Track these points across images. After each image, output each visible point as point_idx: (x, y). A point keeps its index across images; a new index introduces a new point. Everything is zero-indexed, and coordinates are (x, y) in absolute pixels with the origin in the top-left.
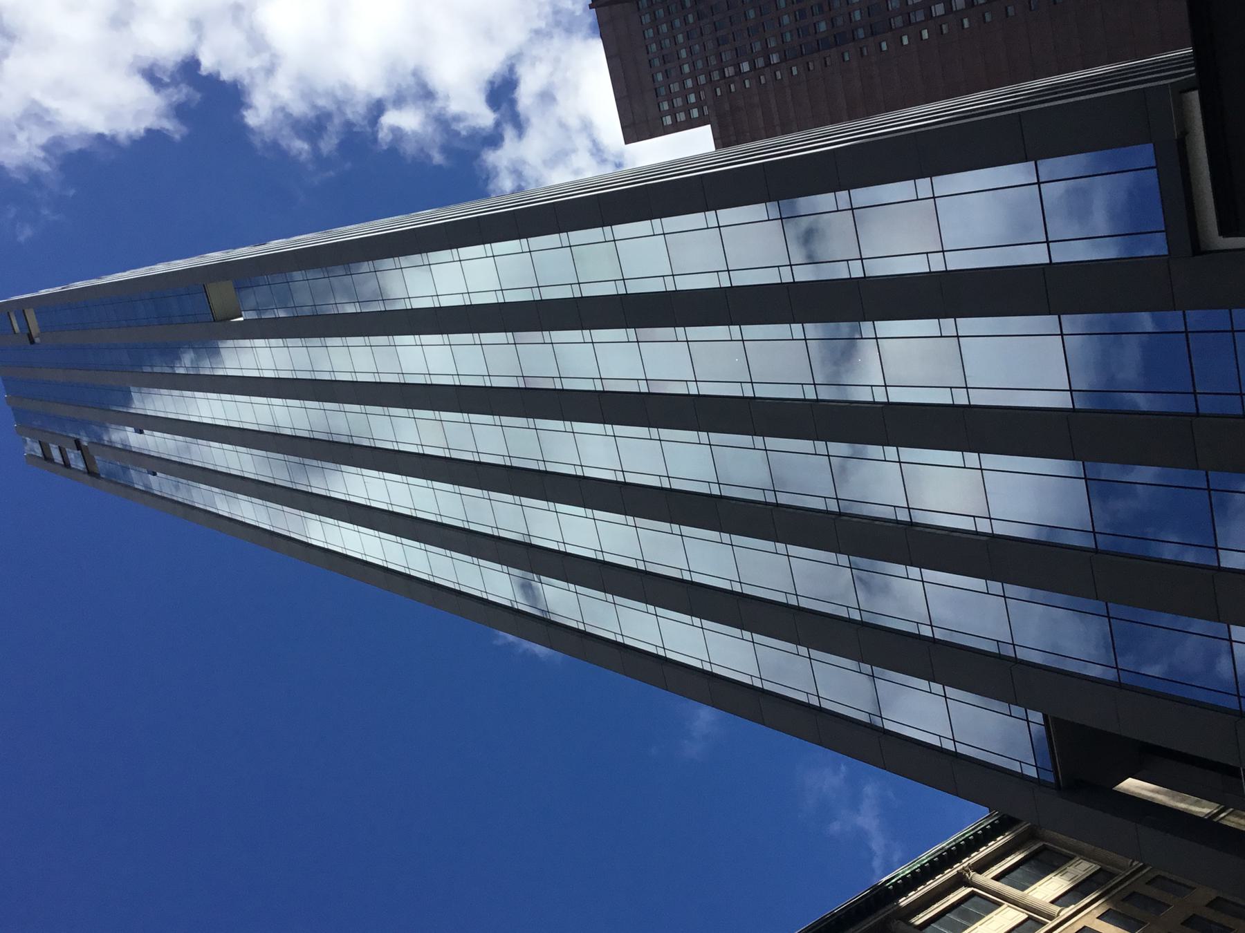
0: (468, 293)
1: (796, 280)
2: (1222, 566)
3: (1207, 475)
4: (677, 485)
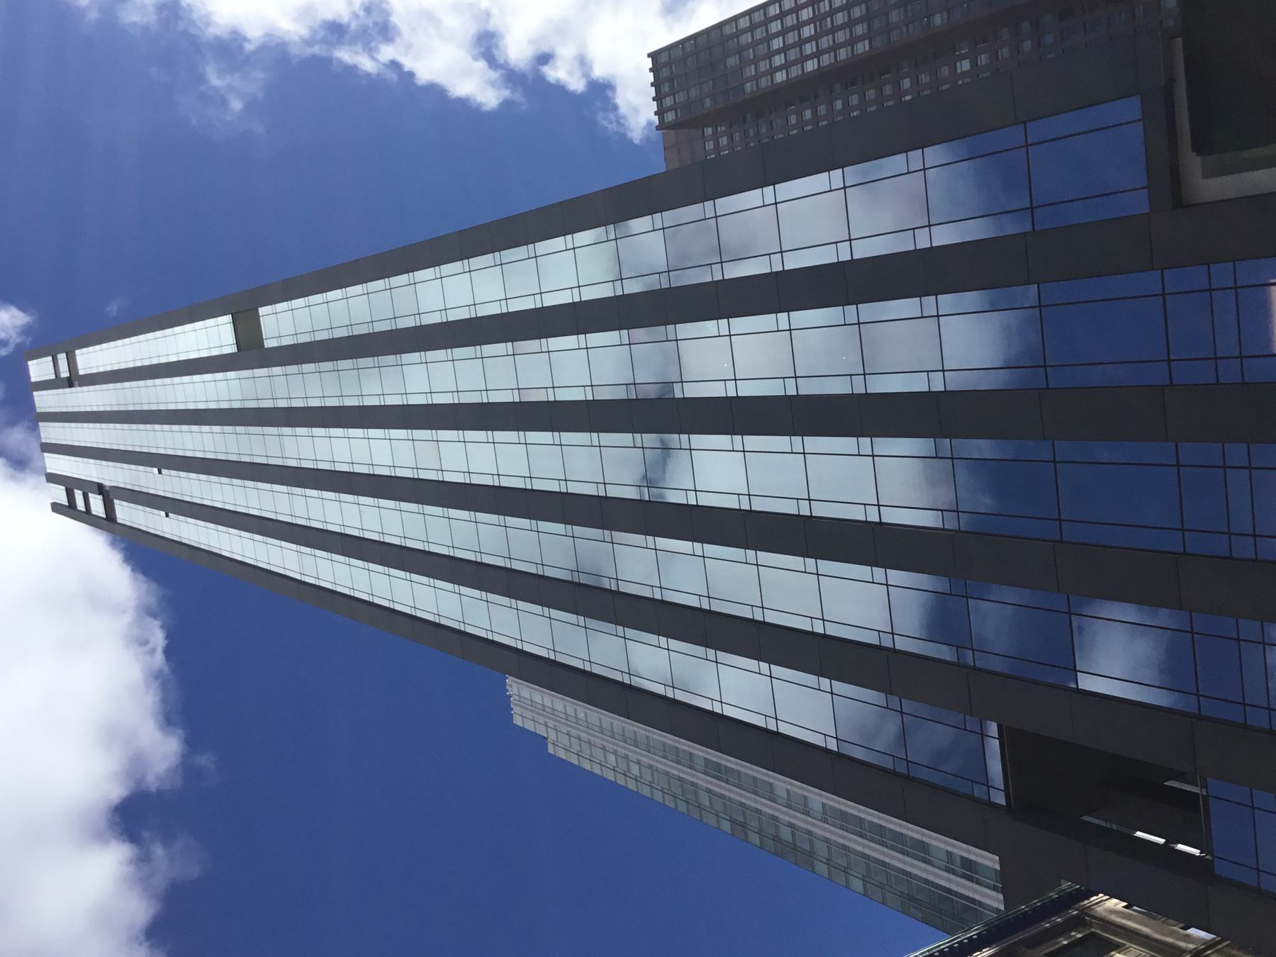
0: (519, 389)
1: (868, 392)
2: (1080, 687)
3: (1237, 621)
4: (833, 631)
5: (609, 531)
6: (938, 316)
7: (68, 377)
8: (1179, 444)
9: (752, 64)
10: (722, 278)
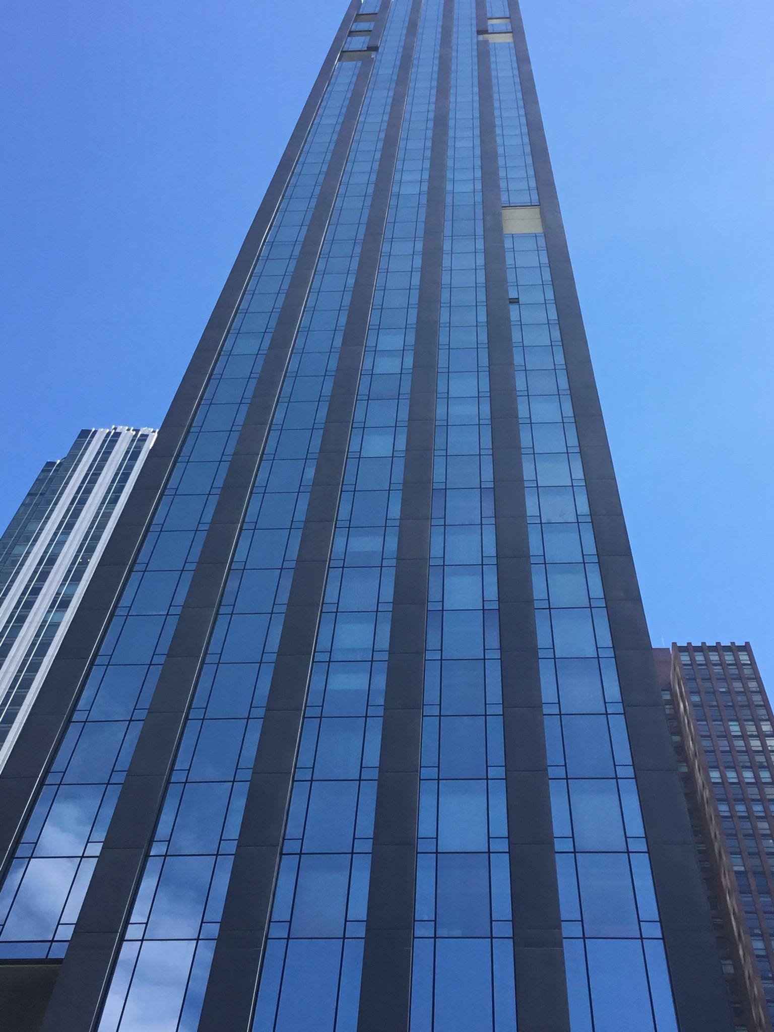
5: (216, 935)
6: (487, 779)
7: (487, 31)
8: (370, 855)
9: (745, 690)
10: (563, 918)
